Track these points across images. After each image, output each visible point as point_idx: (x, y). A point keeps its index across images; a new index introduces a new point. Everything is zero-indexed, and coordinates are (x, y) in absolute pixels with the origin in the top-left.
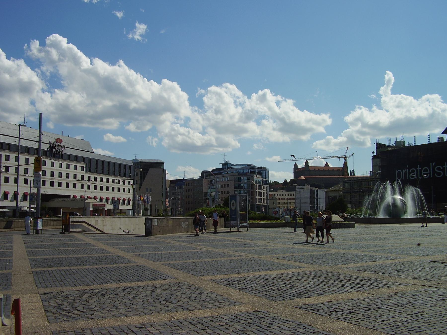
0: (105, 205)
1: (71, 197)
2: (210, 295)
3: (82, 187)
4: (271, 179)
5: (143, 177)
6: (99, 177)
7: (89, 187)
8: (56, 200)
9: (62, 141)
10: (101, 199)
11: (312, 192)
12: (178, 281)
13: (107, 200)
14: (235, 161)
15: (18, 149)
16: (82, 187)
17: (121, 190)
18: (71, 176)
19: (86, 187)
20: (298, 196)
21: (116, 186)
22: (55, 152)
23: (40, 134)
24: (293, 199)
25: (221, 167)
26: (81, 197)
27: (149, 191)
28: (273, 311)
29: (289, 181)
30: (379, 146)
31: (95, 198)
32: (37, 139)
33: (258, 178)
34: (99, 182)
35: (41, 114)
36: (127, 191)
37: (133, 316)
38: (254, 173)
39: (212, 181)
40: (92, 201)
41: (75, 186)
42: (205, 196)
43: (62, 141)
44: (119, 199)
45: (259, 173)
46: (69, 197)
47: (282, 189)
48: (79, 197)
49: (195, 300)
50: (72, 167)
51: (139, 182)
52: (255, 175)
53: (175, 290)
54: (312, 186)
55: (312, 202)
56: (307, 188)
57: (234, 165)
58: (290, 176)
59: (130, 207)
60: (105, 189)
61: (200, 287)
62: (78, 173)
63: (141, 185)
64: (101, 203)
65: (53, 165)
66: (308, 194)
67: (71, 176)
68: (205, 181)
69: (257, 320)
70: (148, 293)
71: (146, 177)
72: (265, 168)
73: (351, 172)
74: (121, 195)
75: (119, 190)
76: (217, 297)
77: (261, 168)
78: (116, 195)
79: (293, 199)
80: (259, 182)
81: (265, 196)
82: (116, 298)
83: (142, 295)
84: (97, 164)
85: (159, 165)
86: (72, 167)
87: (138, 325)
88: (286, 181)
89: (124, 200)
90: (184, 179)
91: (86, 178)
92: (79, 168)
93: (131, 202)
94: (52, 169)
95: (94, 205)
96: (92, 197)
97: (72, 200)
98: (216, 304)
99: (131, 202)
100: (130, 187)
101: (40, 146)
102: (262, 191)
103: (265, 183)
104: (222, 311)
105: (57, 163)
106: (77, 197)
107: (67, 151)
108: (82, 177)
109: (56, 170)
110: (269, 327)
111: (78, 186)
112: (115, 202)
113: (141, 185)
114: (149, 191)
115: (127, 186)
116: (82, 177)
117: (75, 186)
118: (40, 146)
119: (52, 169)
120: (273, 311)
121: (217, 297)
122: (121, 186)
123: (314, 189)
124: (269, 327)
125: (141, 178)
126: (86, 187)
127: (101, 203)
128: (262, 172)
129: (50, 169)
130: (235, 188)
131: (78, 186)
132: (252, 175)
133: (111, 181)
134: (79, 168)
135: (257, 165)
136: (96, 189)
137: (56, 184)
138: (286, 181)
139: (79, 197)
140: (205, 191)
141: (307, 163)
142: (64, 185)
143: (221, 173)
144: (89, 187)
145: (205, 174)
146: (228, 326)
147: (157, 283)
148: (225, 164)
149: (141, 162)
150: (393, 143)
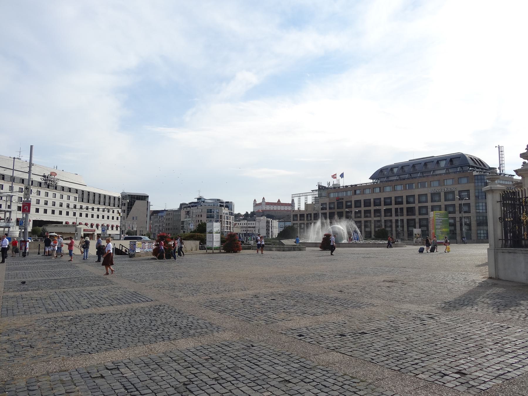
0: (95, 231)
1: (64, 223)
2: (191, 319)
3: (74, 214)
4: (236, 212)
5: (130, 206)
6: (84, 206)
7: (81, 215)
8: (49, 225)
9: (56, 174)
10: (92, 225)
11: (268, 222)
12: (158, 303)
13: (97, 226)
14: (208, 196)
15: (13, 179)
16: (74, 214)
17: (111, 218)
18: (65, 205)
19: (78, 215)
20: (257, 225)
21: (106, 214)
22: (49, 182)
23: (31, 165)
24: (253, 227)
25: (196, 201)
26: (73, 223)
28: (258, 338)
29: (249, 213)
30: (321, 188)
31: (86, 224)
32: (27, 170)
33: (225, 211)
34: (90, 210)
35: (31, 147)
36: (115, 218)
37: (106, 350)
38: (223, 206)
39: (188, 212)
40: (83, 227)
41: (68, 213)
43: (56, 174)
44: (108, 226)
45: (227, 207)
46: (62, 223)
47: (244, 219)
48: (71, 223)
49: (176, 325)
50: (65, 197)
51: (126, 211)
52: (223, 208)
53: (155, 314)
54: (268, 216)
55: (268, 230)
56: (264, 219)
58: (250, 210)
59: (118, 232)
60: (95, 216)
61: (180, 311)
63: (128, 214)
65: (47, 194)
66: (265, 224)
67: (65, 205)
68: (183, 213)
69: (245, 351)
70: (127, 318)
71: (133, 207)
72: (232, 202)
74: (110, 222)
75: (108, 218)
76: (199, 321)
77: (228, 202)
78: (106, 222)
79: (253, 227)
80: (226, 214)
82: (90, 327)
83: (120, 322)
84: (89, 195)
85: (144, 198)
86: (65, 197)
87: (110, 365)
88: (247, 212)
89: (112, 227)
90: (165, 210)
91: (78, 207)
92: (72, 198)
93: (119, 229)
95: (84, 230)
96: (84, 223)
97: (64, 226)
98: (198, 331)
99: (119, 229)
100: (118, 215)
101: (29, 176)
102: (229, 221)
103: (231, 214)
104: (205, 340)
105: (51, 194)
107: (60, 184)
108: (75, 207)
110: (260, 361)
111: (71, 214)
112: (105, 228)
113: (128, 214)
115: (116, 215)
116: (75, 207)
117: (68, 213)
118: (29, 176)
120: (258, 338)
121: (199, 321)
122: (111, 214)
123: (269, 219)
124: (260, 361)
125: (128, 208)
126: (78, 215)
128: (228, 205)
130: (207, 217)
131: (71, 214)
133: (96, 210)
134: (72, 198)
135: (225, 200)
137: (49, 212)
138: (247, 212)
139: (71, 223)
143: (196, 206)
144: (81, 215)
146: (214, 361)
147: (136, 306)
149: (129, 195)
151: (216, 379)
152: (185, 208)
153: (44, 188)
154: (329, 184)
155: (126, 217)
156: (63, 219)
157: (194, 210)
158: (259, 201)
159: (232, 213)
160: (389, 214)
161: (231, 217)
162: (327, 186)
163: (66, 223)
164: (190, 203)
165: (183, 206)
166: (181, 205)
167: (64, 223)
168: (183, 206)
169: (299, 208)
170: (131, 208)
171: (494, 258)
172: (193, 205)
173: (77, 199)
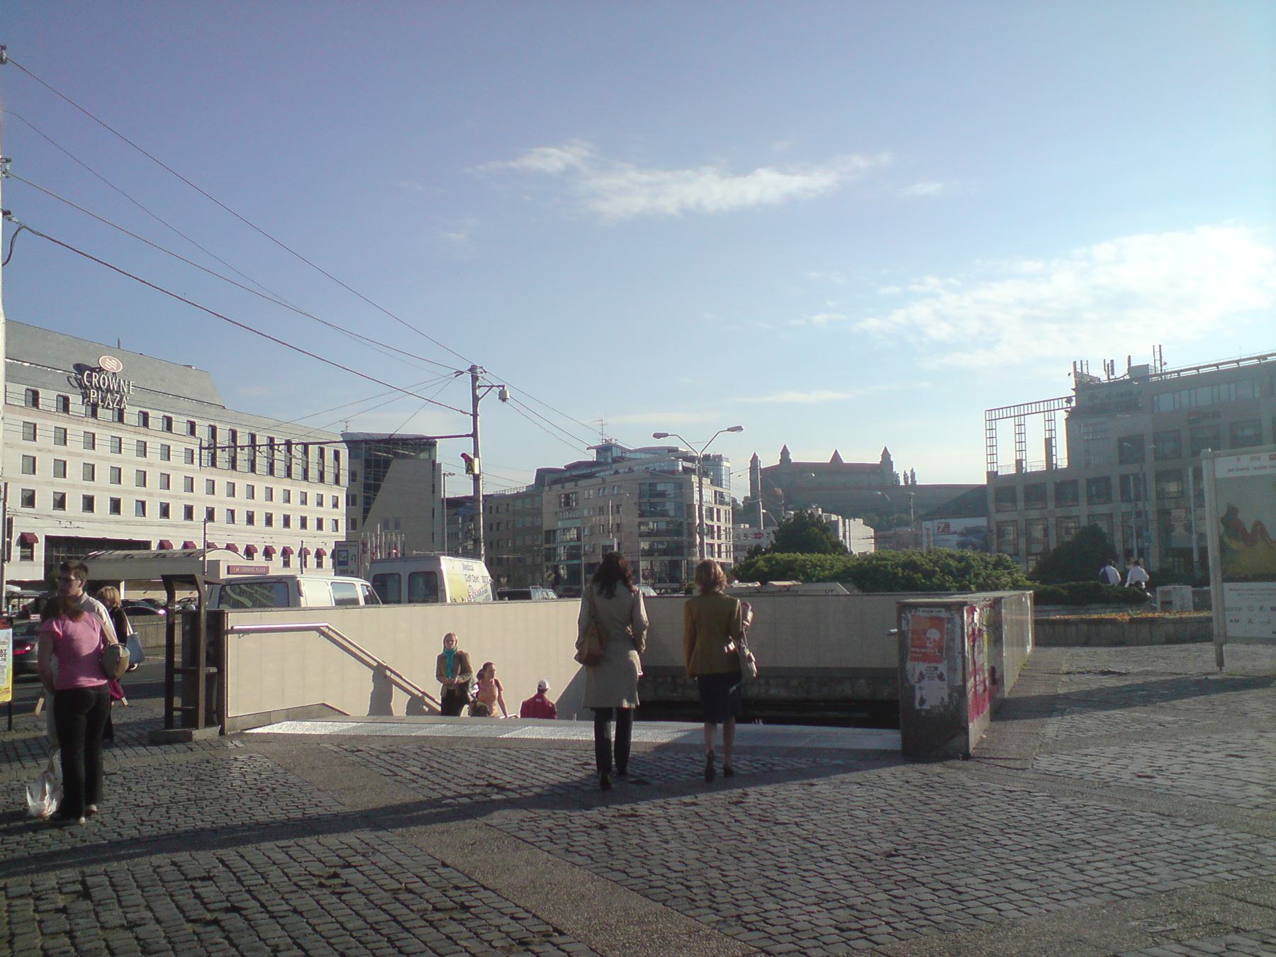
1: (154, 547)
25: (591, 456)
26: (186, 545)
27: (392, 525)
30: (1085, 385)
42: (548, 541)
46: (146, 545)
48: (177, 546)
51: (360, 500)
57: (630, 451)
62: (174, 468)
63: (366, 511)
64: (250, 563)
71: (383, 484)
73: (905, 475)
81: (723, 537)
94: (90, 456)
106: (171, 546)
109: (221, 502)
113: (366, 511)
114: (392, 525)
119: (90, 456)
127: (250, 563)
129: (81, 455)
132: (686, 476)
136: (186, 507)
139: (177, 546)
140: (547, 524)
141: (785, 452)
142: (153, 510)
145: (545, 477)
148: (604, 449)
150: (1121, 372)
151: (376, 851)
152: (555, 482)
153: (79, 419)
154: (1110, 368)
155: (359, 521)
156: (151, 531)
157: (587, 491)
158: (770, 459)
159: (721, 495)
160: (91, 630)
161: (723, 508)
162: (1104, 378)
163: (162, 545)
164: (569, 468)
165: (547, 479)
166: (542, 474)
167: (154, 547)
168: (547, 479)
169: (1019, 463)
170: (377, 488)
171: (1192, 647)
172: (578, 472)
173: (196, 456)
